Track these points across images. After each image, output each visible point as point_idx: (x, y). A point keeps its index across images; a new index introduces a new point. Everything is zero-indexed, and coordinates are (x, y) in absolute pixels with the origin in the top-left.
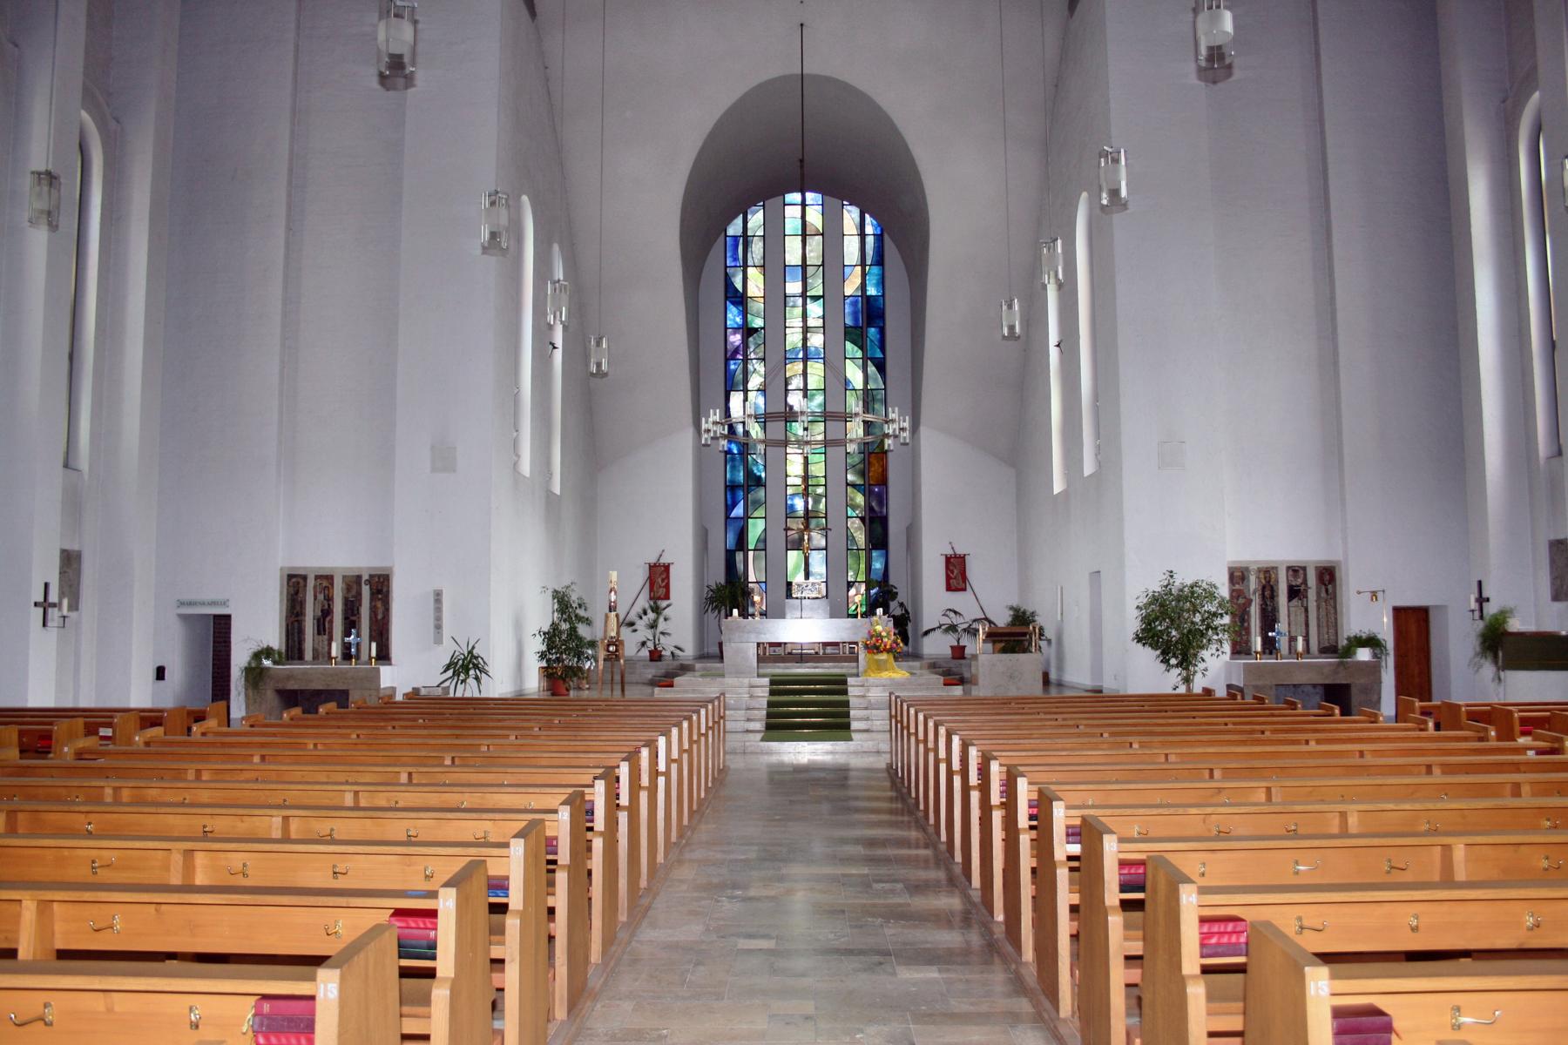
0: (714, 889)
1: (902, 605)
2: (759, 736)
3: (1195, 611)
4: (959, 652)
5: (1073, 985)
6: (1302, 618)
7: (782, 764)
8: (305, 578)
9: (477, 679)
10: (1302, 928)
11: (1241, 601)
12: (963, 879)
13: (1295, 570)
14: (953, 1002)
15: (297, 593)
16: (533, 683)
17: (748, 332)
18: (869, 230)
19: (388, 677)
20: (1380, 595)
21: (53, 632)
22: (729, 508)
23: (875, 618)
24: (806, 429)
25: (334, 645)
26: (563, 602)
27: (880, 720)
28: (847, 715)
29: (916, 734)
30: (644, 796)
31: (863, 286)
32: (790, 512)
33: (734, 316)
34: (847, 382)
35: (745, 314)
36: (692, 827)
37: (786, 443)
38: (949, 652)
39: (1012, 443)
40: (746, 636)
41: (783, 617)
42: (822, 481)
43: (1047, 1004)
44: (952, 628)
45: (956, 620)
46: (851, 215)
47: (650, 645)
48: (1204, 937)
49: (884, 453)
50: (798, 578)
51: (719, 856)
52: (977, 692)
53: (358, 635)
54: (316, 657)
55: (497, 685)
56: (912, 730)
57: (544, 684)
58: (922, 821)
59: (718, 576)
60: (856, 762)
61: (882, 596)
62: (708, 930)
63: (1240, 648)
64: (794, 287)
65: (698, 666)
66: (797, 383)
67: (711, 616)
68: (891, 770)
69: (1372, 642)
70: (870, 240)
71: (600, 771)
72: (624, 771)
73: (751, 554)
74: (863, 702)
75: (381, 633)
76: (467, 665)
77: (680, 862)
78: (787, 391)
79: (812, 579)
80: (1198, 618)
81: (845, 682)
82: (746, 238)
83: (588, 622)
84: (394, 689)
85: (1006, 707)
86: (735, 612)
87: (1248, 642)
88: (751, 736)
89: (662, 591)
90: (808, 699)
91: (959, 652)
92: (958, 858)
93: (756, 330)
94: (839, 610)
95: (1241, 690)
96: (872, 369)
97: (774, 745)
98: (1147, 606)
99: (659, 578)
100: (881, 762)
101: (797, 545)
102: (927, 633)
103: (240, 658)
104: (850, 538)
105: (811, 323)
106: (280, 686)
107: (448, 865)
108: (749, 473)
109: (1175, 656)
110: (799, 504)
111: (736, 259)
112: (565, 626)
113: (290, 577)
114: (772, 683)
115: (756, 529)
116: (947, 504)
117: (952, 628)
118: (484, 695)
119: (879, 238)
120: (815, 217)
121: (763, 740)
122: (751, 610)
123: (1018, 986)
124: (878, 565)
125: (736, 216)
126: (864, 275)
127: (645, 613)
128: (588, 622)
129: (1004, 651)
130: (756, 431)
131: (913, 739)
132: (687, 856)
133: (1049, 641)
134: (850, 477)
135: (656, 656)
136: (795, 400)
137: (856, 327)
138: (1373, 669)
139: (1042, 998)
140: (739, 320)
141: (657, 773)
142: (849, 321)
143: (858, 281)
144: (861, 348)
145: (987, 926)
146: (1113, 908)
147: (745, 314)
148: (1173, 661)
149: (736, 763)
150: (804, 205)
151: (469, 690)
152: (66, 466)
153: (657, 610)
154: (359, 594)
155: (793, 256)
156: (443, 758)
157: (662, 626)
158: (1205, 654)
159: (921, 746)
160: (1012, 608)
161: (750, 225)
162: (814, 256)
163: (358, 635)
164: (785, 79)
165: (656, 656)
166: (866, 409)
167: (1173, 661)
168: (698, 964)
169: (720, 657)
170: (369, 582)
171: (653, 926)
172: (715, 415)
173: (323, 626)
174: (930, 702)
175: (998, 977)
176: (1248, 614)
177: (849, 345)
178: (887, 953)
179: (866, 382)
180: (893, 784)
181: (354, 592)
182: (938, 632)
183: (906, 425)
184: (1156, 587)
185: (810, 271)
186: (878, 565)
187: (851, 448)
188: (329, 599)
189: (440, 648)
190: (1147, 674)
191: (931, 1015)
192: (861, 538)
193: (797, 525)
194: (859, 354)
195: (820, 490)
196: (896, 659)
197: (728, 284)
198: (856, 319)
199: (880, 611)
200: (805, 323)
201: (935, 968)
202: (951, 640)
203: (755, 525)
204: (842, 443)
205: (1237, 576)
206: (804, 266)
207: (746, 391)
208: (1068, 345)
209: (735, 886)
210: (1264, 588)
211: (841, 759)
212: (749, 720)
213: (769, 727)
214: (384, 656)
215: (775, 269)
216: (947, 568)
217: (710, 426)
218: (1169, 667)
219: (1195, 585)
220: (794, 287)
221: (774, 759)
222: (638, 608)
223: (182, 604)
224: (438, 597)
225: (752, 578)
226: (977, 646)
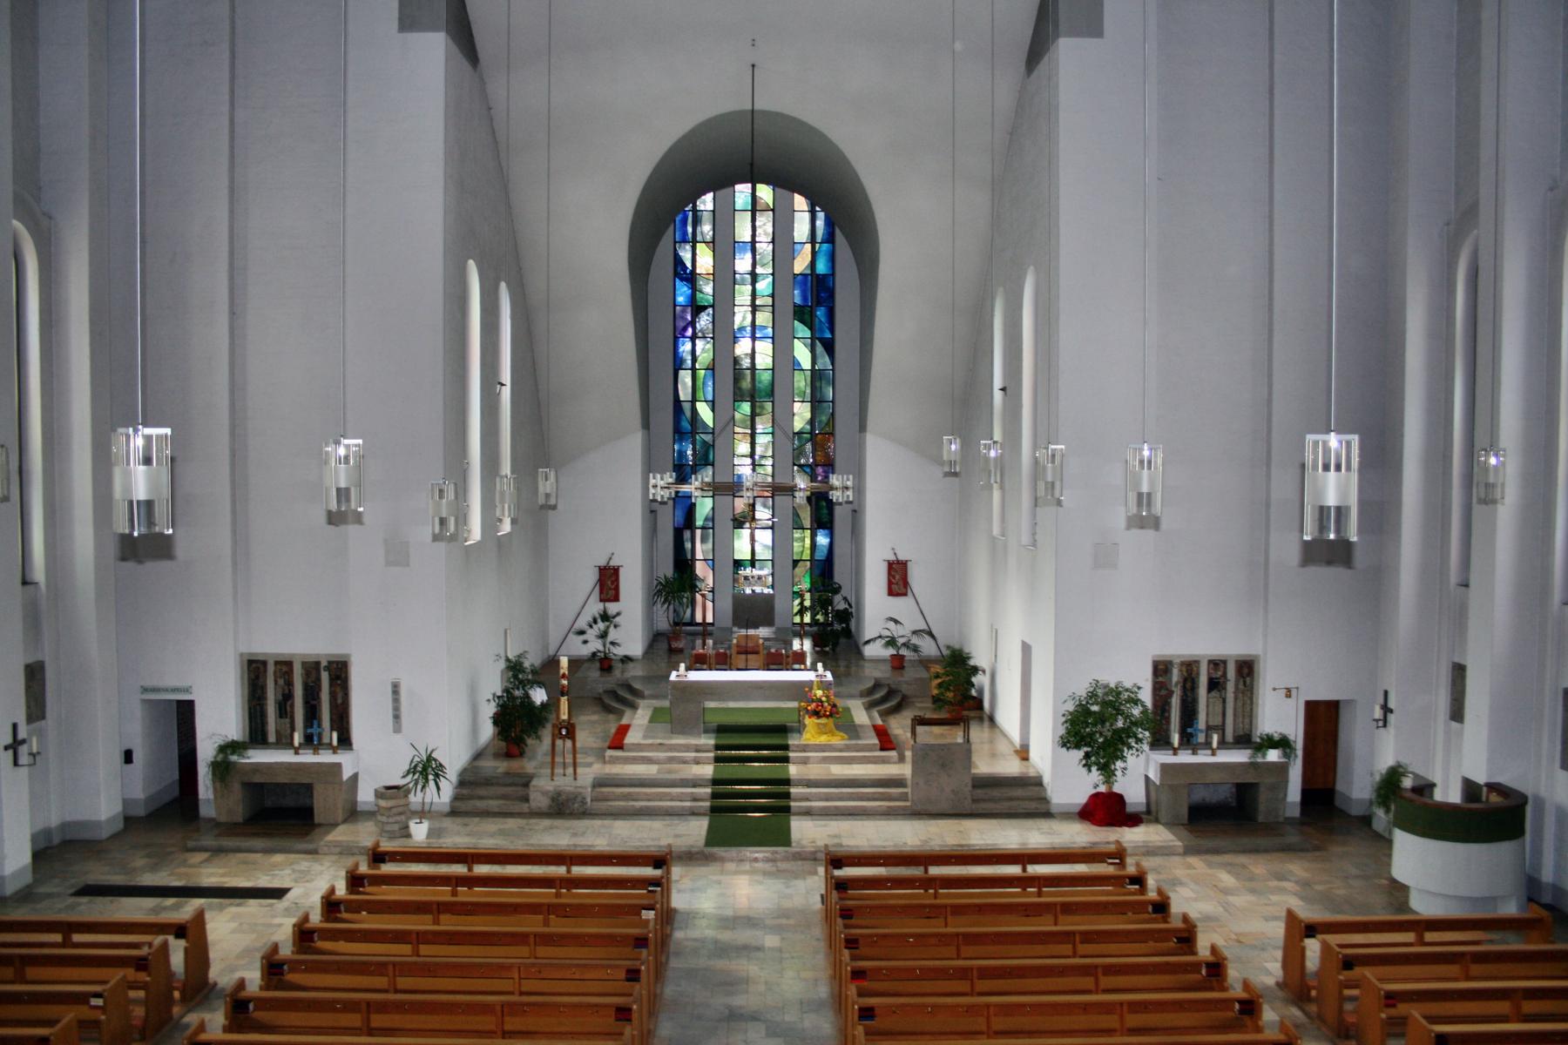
1: (845, 599)
6: (1219, 709)
8: (264, 663)
11: (1163, 692)
13: (1217, 664)
15: (257, 677)
20: (1294, 692)
21: (23, 772)
42: (770, 330)
46: (800, 202)
59: (667, 569)
66: (743, 447)
69: (1283, 743)
73: (698, 532)
89: (612, 593)
96: (819, 348)
102: (868, 642)
103: (206, 751)
106: (246, 779)
113: (250, 662)
126: (814, 253)
138: (1281, 770)
142: (798, 300)
143: (809, 258)
144: (811, 328)
152: (25, 583)
154: (319, 679)
155: (743, 232)
163: (320, 726)
164: (741, 113)
170: (327, 668)
173: (284, 708)
176: (1169, 704)
179: (814, 362)
183: (849, 483)
188: (290, 683)
194: (808, 334)
197: (678, 262)
198: (804, 298)
205: (1161, 669)
208: (1011, 390)
210: (1185, 680)
214: (345, 742)
215: (724, 247)
223: (145, 690)
224: (396, 689)
225: (699, 555)
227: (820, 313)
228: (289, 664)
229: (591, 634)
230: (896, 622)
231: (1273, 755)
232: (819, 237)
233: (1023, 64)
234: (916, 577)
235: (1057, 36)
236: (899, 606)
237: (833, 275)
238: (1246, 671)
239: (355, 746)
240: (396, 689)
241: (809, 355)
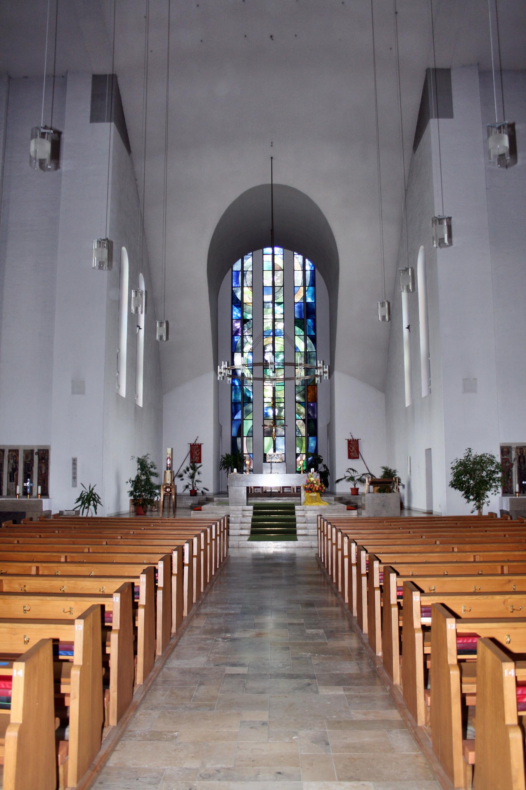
0: (213, 632)
1: (325, 466)
2: (247, 538)
3: (483, 470)
4: (355, 491)
5: (426, 706)
7: (259, 554)
9: (95, 507)
10: (513, 610)
11: (507, 464)
12: (358, 627)
14: (353, 712)
16: (126, 506)
17: (244, 321)
18: (308, 268)
19: (46, 505)
22: (234, 414)
23: (310, 474)
24: (274, 372)
25: (18, 487)
26: (142, 464)
27: (312, 529)
28: (295, 526)
29: (331, 539)
30: (195, 560)
31: (304, 297)
32: (265, 416)
33: (236, 313)
34: (296, 348)
35: (242, 312)
36: (206, 593)
37: (264, 379)
38: (349, 491)
39: (383, 378)
40: (241, 483)
41: (262, 473)
42: (283, 400)
43: (410, 716)
44: (352, 479)
45: (353, 474)
46: (298, 259)
47: (191, 487)
48: (519, 698)
49: (316, 385)
50: (270, 452)
51: (219, 611)
52: (364, 514)
53: (31, 482)
54: (9, 494)
55: (106, 509)
56: (329, 537)
57: (133, 509)
58: (335, 589)
59: (227, 450)
60: (300, 553)
61: (314, 461)
62: (209, 660)
63: (507, 491)
64: (268, 298)
65: (215, 499)
66: (269, 348)
67: (224, 471)
68: (318, 558)
70: (308, 273)
71: (175, 547)
72: (187, 547)
73: (245, 439)
74: (304, 520)
75: (44, 481)
76: (89, 498)
77: (198, 615)
78: (264, 352)
79: (277, 452)
80: (484, 474)
81: (294, 508)
82: (243, 272)
83: (156, 475)
84: (50, 511)
85: (380, 523)
86: (235, 470)
87: (511, 486)
88: (243, 538)
89: (197, 458)
90: (274, 517)
91: (355, 491)
92: (355, 614)
93: (248, 320)
94: (292, 469)
95: (507, 513)
96: (309, 341)
97: (255, 543)
98: (457, 467)
99: (195, 451)
100: (312, 553)
101: (269, 434)
104: (296, 429)
105: (277, 317)
107: (119, 583)
108: (244, 396)
109: (473, 495)
110: (270, 412)
111: (237, 283)
112: (143, 477)
114: (254, 508)
115: (248, 425)
116: (349, 410)
117: (352, 479)
118: (99, 515)
119: (313, 272)
120: (279, 261)
121: (249, 540)
122: (245, 468)
123: (391, 701)
124: (312, 444)
125: (237, 260)
126: (305, 291)
127: (188, 470)
128: (156, 475)
129: (380, 491)
130: (247, 373)
131: (330, 542)
132: (203, 611)
133: (404, 486)
134: (298, 398)
135: (194, 493)
136: (269, 357)
137: (301, 319)
139: (407, 711)
140: (239, 315)
141: (201, 550)
142: (297, 316)
144: (303, 330)
145: (373, 657)
146: (452, 665)
147: (242, 312)
148: (471, 497)
149: (233, 553)
150: (273, 254)
151: (90, 512)
153: (194, 468)
154: (32, 460)
155: (268, 282)
156: (60, 557)
157: (197, 477)
158: (488, 493)
159: (334, 547)
160: (383, 468)
161: (245, 265)
162: (279, 282)
165: (194, 493)
166: (306, 361)
167: (471, 497)
168: (201, 684)
169: (226, 494)
170: (38, 453)
171: (178, 657)
172: (224, 365)
174: (340, 521)
175: (378, 692)
176: (511, 471)
177: (297, 329)
178: (313, 677)
180: (319, 566)
181: (29, 459)
182: (344, 481)
184: (462, 457)
185: (277, 289)
186: (312, 444)
187: (298, 382)
188: (16, 462)
189: (76, 489)
190: (460, 506)
191: (339, 722)
192: (303, 430)
193: (268, 423)
194: (302, 333)
195: (282, 405)
196: (321, 496)
199: (312, 470)
200: (274, 317)
201: (341, 688)
202: (351, 485)
203: (247, 423)
204: (294, 379)
205: (505, 450)
206: (274, 286)
207: (242, 353)
208: (412, 327)
209: (227, 631)
210: (520, 457)
211: (291, 551)
212: (241, 529)
213: (253, 533)
214: (45, 493)
215: (258, 289)
216: (349, 447)
217: (223, 371)
218: (469, 500)
219: (483, 455)
220: (268, 298)
221: (255, 551)
222: (184, 468)
224: (74, 462)
225: (245, 451)
226: (363, 489)
228: (16, 451)
229: (186, 476)
230: (353, 470)
232: (307, 285)
233: (412, 150)
234: (363, 448)
235: (429, 119)
237: (315, 302)
239: (50, 496)
240: (74, 462)
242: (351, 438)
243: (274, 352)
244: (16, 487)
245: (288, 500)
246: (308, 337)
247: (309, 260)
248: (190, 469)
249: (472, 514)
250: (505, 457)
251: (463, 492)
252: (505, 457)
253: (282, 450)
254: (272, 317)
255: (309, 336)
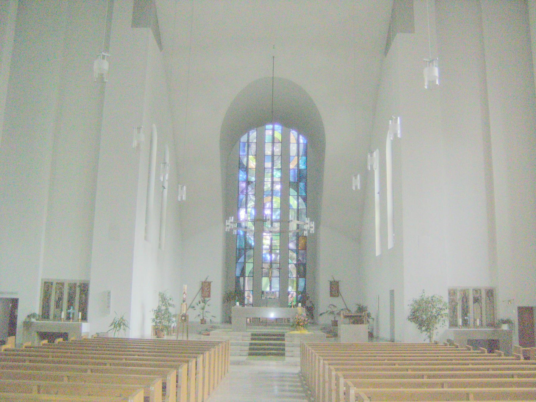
11: (453, 303)
17: (248, 183)
18: (301, 141)
25: (63, 313)
31: (298, 165)
42: (278, 248)
44: (332, 313)
46: (293, 135)
53: (74, 309)
54: (55, 317)
59: (232, 289)
61: (304, 298)
64: (268, 165)
66: (268, 205)
73: (246, 278)
75: (84, 309)
83: (173, 306)
89: (207, 294)
93: (252, 182)
96: (301, 200)
101: (267, 275)
110: (268, 257)
112: (163, 308)
113: (45, 283)
117: (332, 313)
119: (306, 146)
120: (278, 135)
128: (173, 306)
129: (354, 323)
133: (373, 319)
135: (203, 321)
147: (247, 174)
150: (273, 130)
151: (120, 334)
155: (268, 152)
160: (357, 305)
165: (203, 321)
173: (58, 305)
184: (418, 298)
185: (275, 158)
199: (300, 304)
200: (273, 180)
205: (452, 293)
207: (246, 208)
214: (84, 318)
215: (260, 157)
220: (268, 165)
227: (302, 184)
228: (63, 284)
230: (334, 306)
231: (505, 327)
232: (301, 154)
236: (337, 301)
238: (490, 294)
241: (296, 202)
242: (333, 280)
243: (272, 208)
244: (61, 312)
245: (280, 329)
246: (300, 197)
247: (303, 136)
248: (201, 302)
249: (424, 342)
250: (452, 297)
251: (417, 325)
252: (452, 297)
253: (277, 288)
254: (270, 180)
255: (301, 196)
